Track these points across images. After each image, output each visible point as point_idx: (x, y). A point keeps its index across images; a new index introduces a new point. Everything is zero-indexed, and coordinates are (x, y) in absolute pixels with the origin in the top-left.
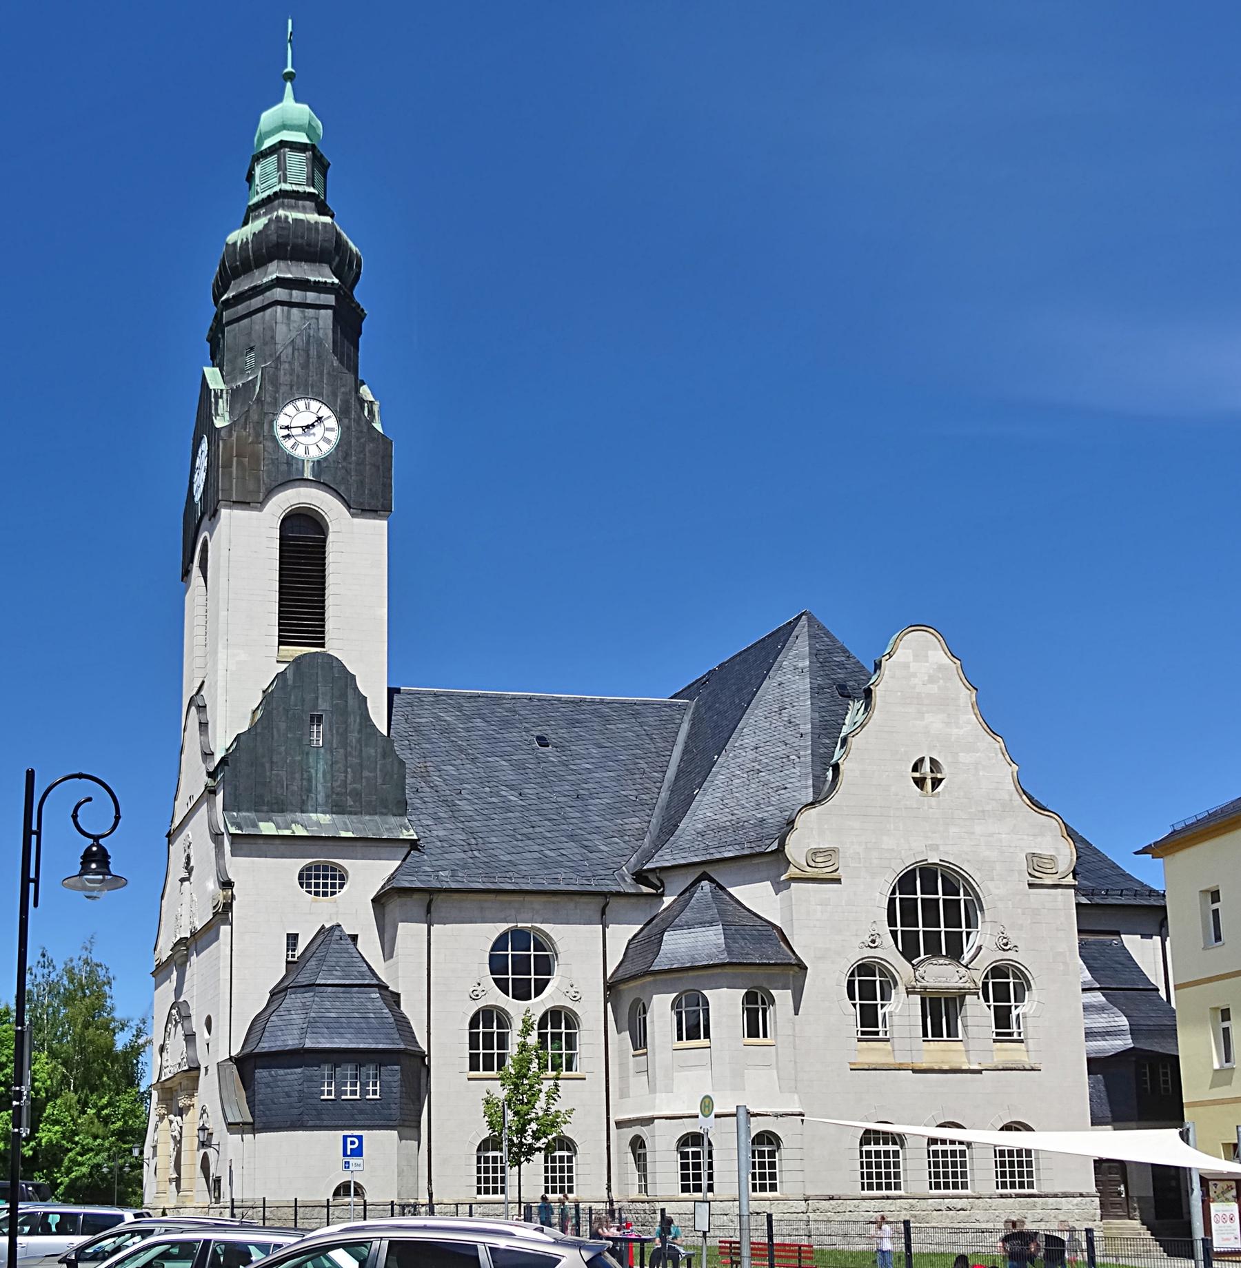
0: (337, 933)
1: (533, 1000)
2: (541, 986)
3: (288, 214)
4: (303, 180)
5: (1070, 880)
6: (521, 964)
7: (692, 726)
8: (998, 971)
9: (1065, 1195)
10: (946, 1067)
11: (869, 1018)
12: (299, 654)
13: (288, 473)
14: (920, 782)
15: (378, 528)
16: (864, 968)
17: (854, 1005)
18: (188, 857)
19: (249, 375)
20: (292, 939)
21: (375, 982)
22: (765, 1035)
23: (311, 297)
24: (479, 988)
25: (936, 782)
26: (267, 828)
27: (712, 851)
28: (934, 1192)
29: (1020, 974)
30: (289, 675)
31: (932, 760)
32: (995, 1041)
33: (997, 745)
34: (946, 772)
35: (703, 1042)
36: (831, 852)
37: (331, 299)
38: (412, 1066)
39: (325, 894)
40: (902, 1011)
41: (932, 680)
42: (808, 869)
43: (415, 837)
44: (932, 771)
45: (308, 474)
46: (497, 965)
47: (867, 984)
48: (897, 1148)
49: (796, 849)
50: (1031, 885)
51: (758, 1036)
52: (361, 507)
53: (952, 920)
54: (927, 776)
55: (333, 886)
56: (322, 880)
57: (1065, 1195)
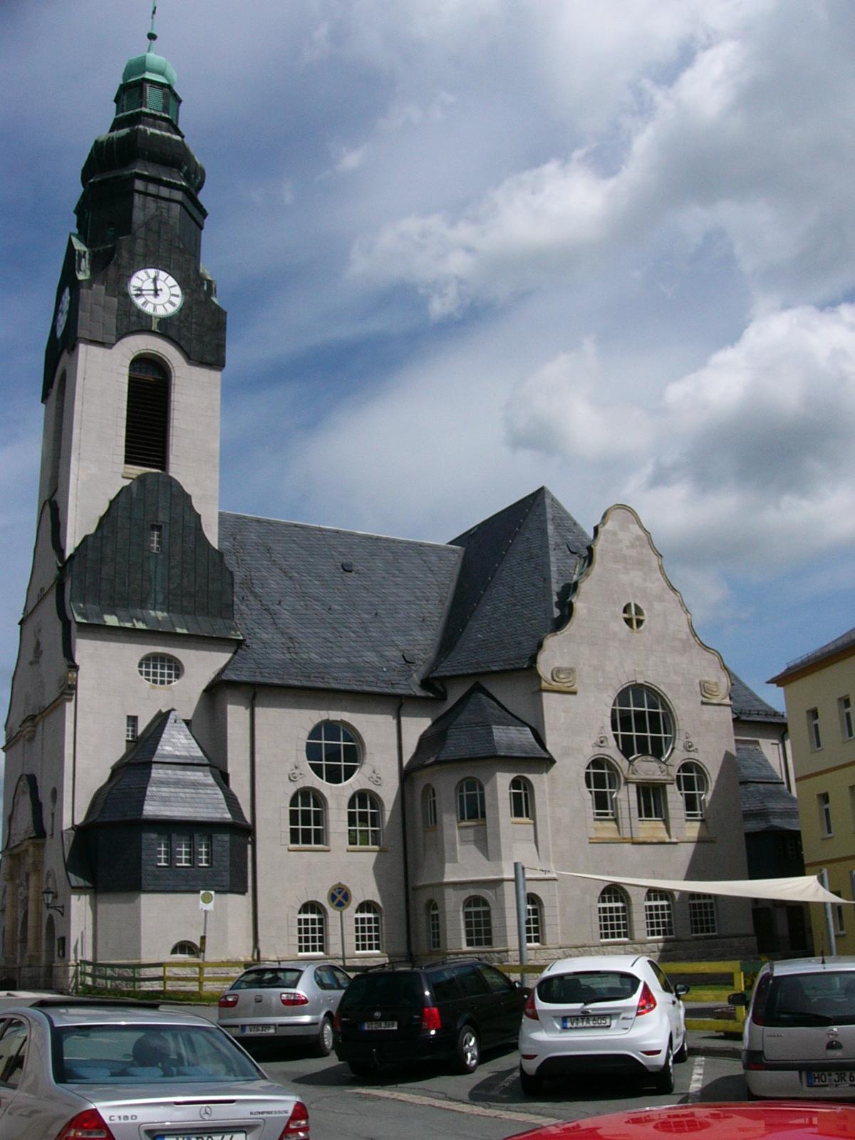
1: (345, 783)
2: (350, 772)
3: (147, 128)
4: (160, 109)
5: (727, 701)
6: (335, 753)
7: (225, 1055)
8: (686, 767)
10: (655, 841)
11: (601, 802)
12: (139, 473)
13: (134, 321)
14: (628, 621)
15: (213, 377)
16: (597, 763)
17: (591, 792)
18: (38, 644)
19: (108, 244)
20: (133, 720)
23: (164, 192)
24: (297, 772)
25: (640, 623)
26: (111, 620)
27: (482, 665)
28: (650, 938)
30: (134, 489)
31: (637, 607)
32: (687, 820)
33: (677, 598)
34: (646, 617)
36: (571, 671)
37: (178, 195)
38: (241, 832)
39: (162, 682)
40: (626, 798)
41: (632, 546)
42: (554, 683)
43: (241, 638)
44: (636, 614)
45: (154, 327)
46: (312, 752)
47: (600, 777)
50: (703, 703)
52: (195, 359)
54: (633, 617)
55: (170, 675)
56: (163, 668)
57: (736, 936)
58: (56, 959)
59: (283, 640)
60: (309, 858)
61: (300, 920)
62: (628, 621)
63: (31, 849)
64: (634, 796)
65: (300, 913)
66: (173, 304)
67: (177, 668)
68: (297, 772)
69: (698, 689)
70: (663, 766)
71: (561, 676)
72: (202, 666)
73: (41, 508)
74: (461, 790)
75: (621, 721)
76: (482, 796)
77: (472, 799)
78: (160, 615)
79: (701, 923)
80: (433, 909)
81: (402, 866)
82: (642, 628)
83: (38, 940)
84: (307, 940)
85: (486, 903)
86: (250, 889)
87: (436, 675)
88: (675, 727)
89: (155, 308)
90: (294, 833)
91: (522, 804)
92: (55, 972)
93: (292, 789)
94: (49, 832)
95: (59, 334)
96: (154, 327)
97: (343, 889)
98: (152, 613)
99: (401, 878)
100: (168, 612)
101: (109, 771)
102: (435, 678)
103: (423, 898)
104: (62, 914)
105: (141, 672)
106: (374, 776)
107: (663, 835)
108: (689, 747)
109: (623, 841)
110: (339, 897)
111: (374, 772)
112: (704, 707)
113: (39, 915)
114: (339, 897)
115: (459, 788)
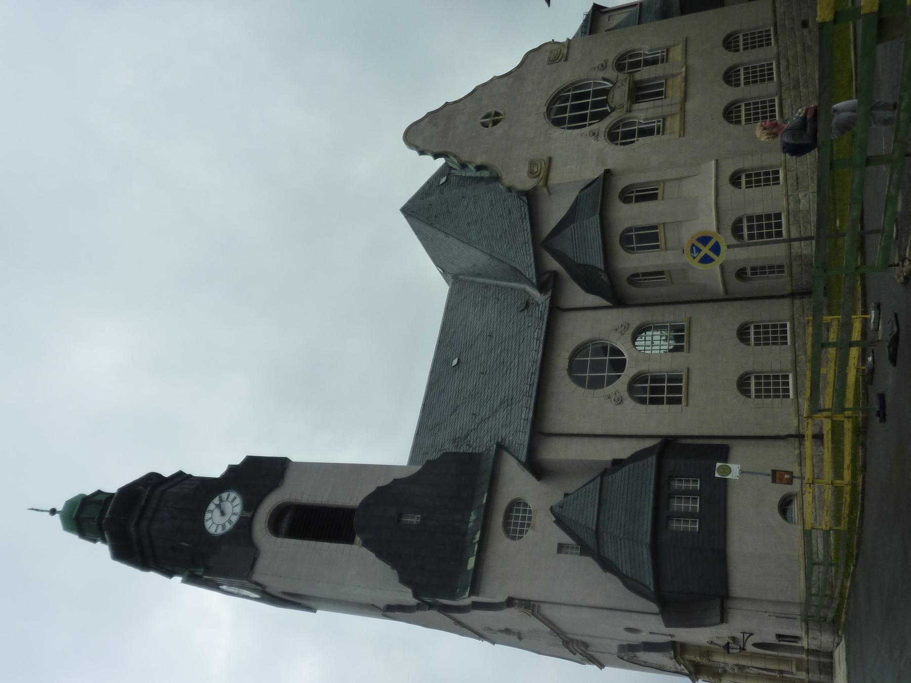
0: (557, 510)
1: (626, 356)
2: (616, 352)
6: (599, 364)
9: (774, 11)
11: (646, 132)
21: (599, 479)
22: (657, 189)
24: (613, 397)
25: (497, 114)
29: (622, 57)
34: (492, 110)
35: (660, 231)
36: (532, 163)
38: (668, 447)
39: (530, 519)
40: (643, 113)
42: (541, 176)
46: (596, 384)
47: (622, 135)
48: (743, 105)
49: (524, 182)
50: (566, 60)
51: (657, 194)
53: (585, 95)
56: (517, 518)
57: (774, 11)
58: (799, 644)
59: (502, 410)
60: (696, 388)
61: (757, 397)
62: (495, 123)
63: (687, 657)
64: (643, 105)
65: (750, 397)
66: (235, 498)
67: (516, 505)
68: (613, 397)
69: (554, 65)
70: (618, 84)
71: (535, 170)
72: (516, 481)
73: (459, 628)
74: (632, 249)
75: (578, 121)
76: (638, 229)
77: (641, 239)
78: (473, 517)
79: (766, 112)
80: (746, 274)
81: (703, 305)
82: (501, 112)
83: (780, 660)
84: (777, 391)
85: (739, 221)
86: (725, 442)
87: (535, 281)
88: (584, 80)
89: (234, 514)
90: (671, 401)
91: (648, 194)
92: (813, 647)
93: (629, 403)
94: (669, 639)
95: (258, 596)
96: (249, 515)
97: (693, 245)
98: (471, 525)
99: (716, 306)
100: (470, 511)
101: (608, 574)
102: (538, 281)
103: (737, 286)
104: (751, 634)
105: (520, 538)
106: (620, 330)
107: (679, 80)
108: (603, 67)
109: (683, 110)
110: (706, 250)
111: (616, 330)
112: (570, 58)
113: (753, 656)
114: (706, 250)
115: (631, 250)
